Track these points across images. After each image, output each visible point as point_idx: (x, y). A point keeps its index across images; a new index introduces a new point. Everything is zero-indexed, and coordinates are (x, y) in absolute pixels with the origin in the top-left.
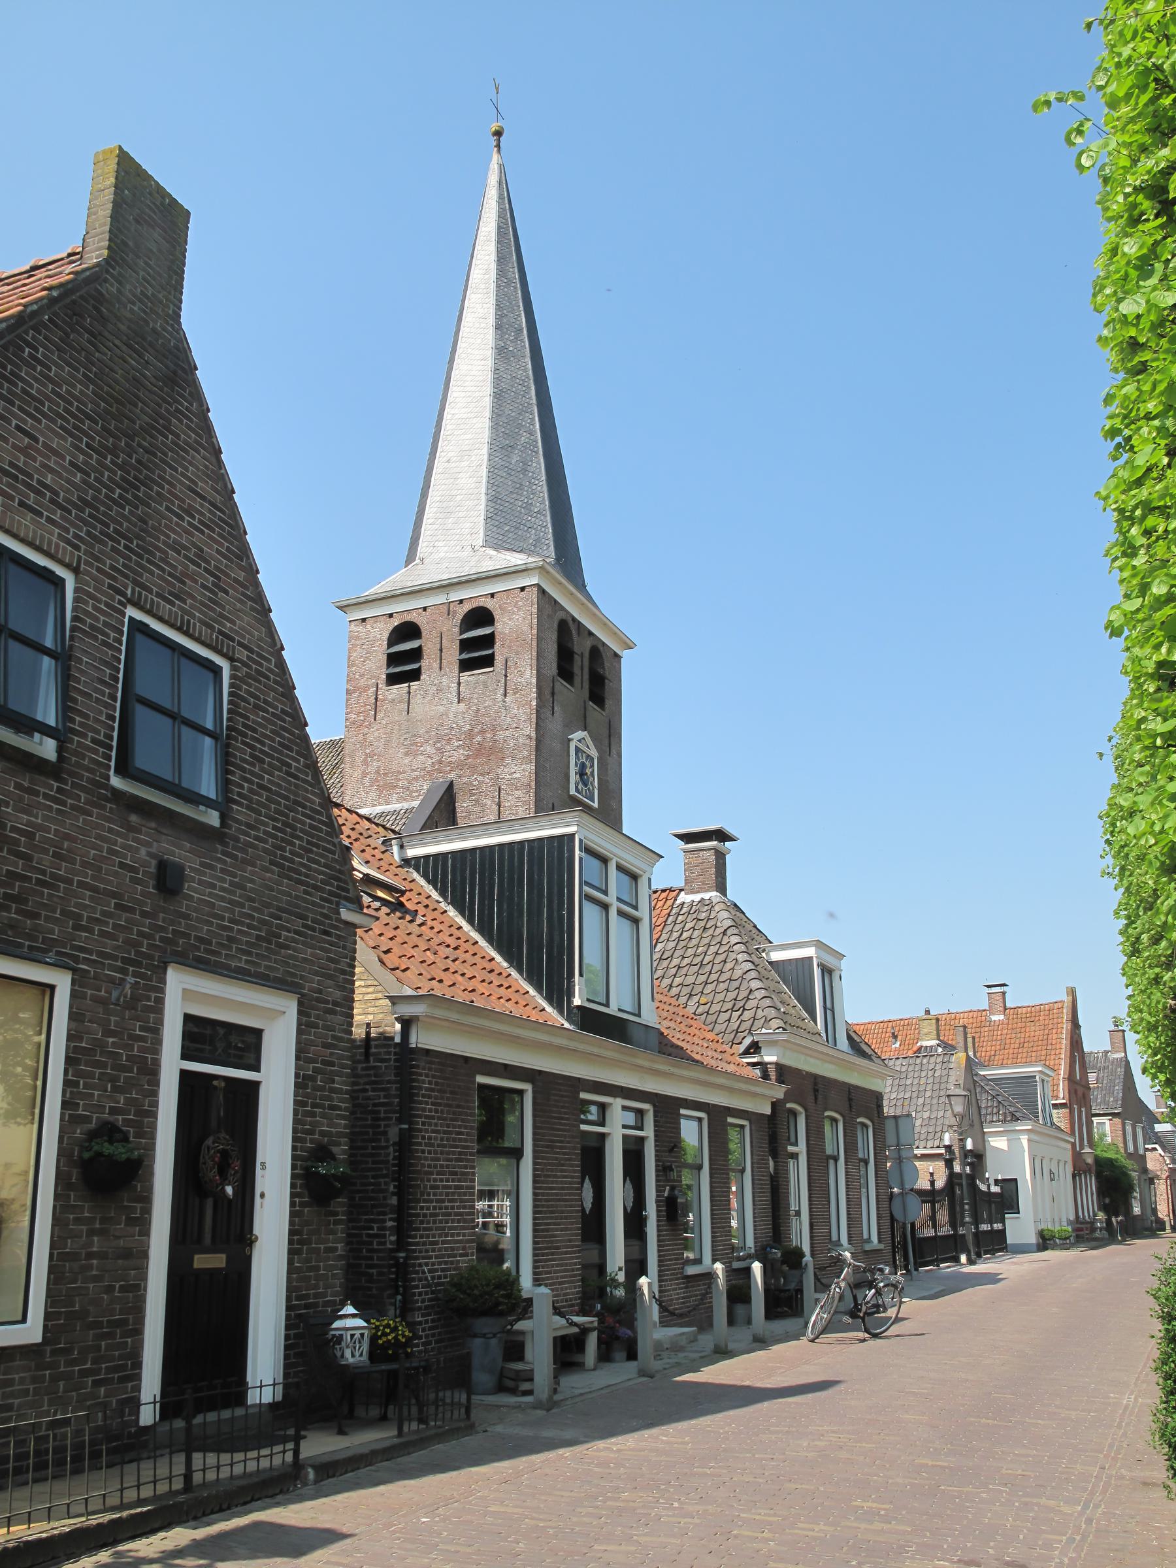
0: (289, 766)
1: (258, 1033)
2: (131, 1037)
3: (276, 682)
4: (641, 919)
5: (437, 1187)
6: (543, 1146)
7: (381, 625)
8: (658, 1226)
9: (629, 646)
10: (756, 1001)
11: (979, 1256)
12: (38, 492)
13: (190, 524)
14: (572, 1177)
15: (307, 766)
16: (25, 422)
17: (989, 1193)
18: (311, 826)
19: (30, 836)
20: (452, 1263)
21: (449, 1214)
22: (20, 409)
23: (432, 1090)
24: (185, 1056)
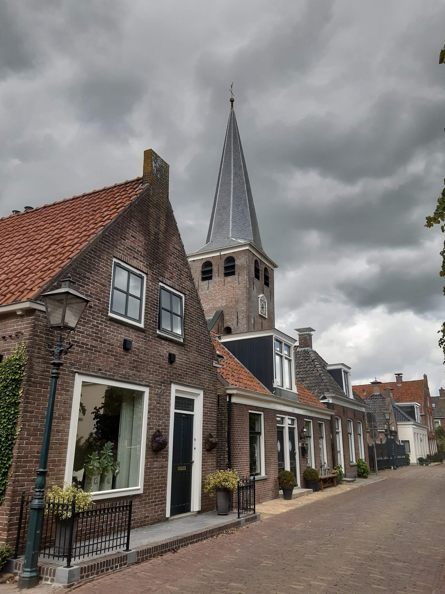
0: (200, 323)
1: (193, 400)
2: (163, 404)
3: (196, 299)
4: (291, 360)
5: (239, 445)
6: (267, 431)
7: (199, 262)
8: (299, 456)
9: (276, 266)
10: (324, 383)
11: (397, 466)
12: (137, 253)
13: (174, 257)
14: (275, 441)
15: (204, 322)
16: (133, 234)
17: (400, 445)
18: (205, 340)
19: (138, 349)
20: (244, 468)
21: (243, 453)
22: (132, 230)
23: (238, 415)
24: (175, 409)
